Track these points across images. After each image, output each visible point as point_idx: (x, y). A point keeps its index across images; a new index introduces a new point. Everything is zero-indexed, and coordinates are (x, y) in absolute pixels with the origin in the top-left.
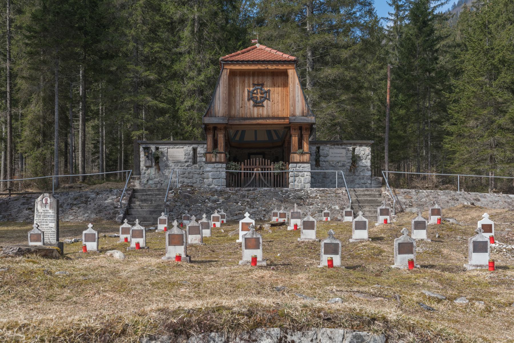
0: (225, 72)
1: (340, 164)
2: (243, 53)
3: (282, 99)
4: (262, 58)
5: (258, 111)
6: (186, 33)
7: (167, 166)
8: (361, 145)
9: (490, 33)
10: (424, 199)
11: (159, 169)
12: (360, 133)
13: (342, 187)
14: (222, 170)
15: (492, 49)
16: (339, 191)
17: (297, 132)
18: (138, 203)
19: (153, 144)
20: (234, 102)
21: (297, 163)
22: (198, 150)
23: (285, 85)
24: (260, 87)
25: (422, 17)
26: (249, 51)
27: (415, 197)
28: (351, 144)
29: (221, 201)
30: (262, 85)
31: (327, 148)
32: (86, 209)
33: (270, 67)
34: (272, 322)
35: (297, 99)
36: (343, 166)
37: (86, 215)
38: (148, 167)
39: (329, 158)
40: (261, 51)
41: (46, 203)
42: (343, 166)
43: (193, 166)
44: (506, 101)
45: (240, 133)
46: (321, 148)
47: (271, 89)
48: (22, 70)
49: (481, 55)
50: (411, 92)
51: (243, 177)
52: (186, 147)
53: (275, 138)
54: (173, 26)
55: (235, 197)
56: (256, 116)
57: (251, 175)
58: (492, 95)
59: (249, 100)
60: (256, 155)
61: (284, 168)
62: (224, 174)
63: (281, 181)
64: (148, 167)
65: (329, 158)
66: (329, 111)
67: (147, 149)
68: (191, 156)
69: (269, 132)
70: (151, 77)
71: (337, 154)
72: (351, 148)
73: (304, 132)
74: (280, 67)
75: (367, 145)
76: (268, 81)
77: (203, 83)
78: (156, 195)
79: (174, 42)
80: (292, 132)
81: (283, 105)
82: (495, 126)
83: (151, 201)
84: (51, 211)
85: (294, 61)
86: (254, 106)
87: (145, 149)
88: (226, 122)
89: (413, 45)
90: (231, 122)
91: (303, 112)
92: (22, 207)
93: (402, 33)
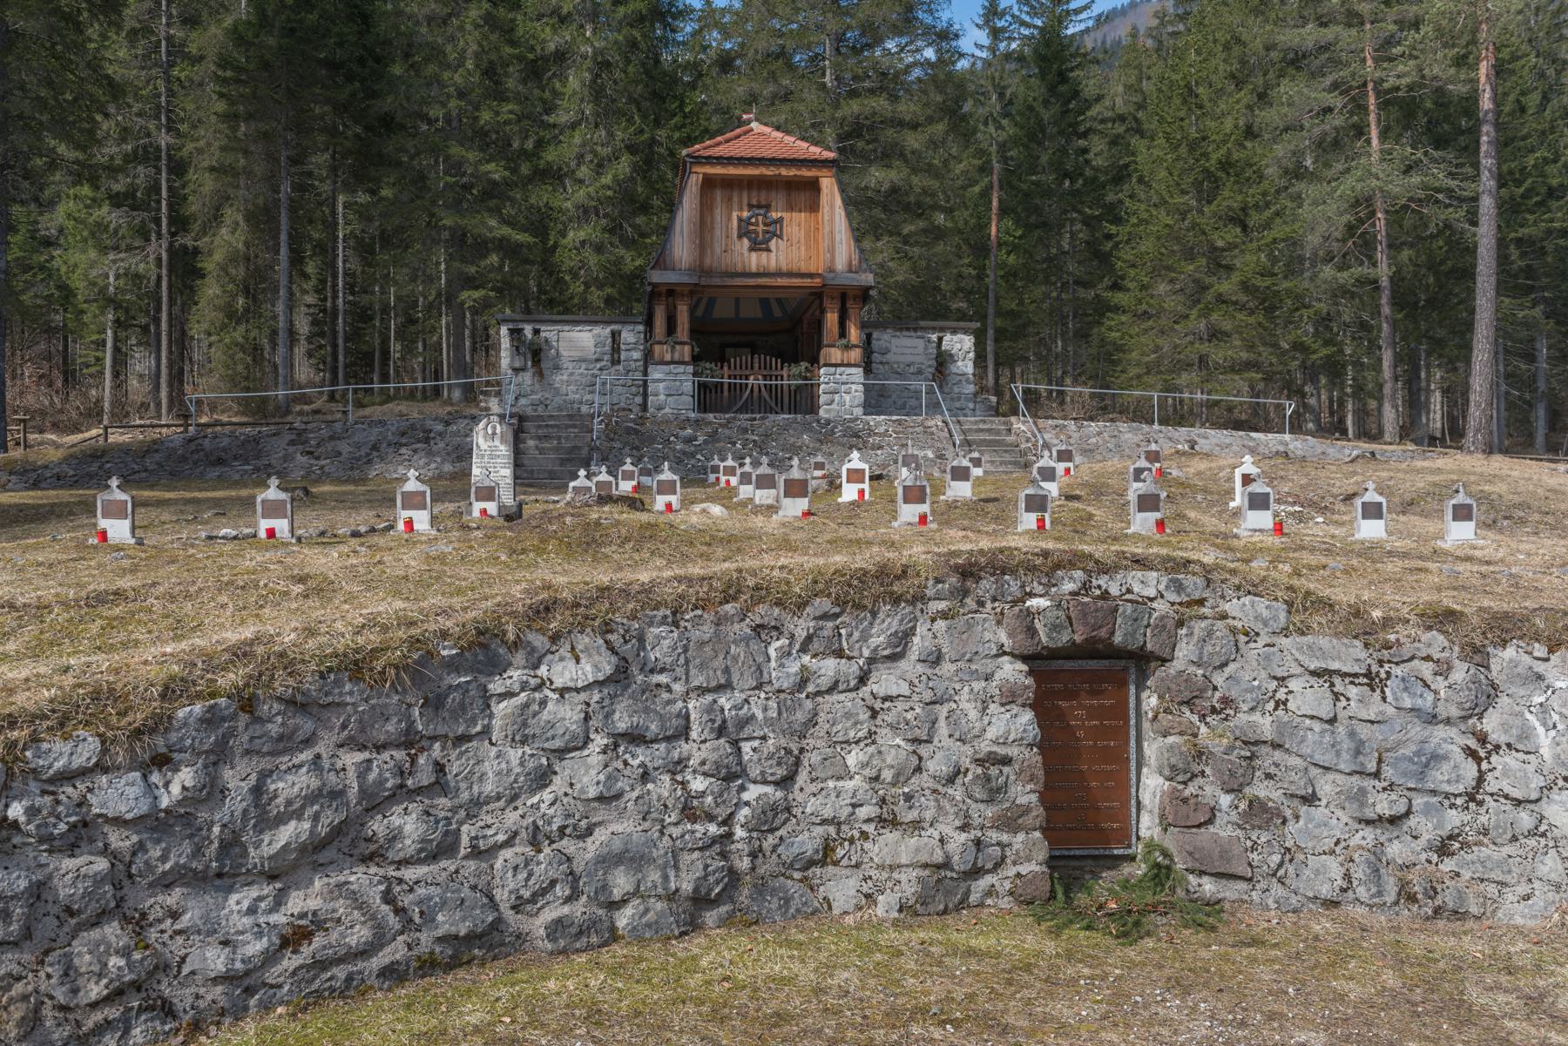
0: (694, 178)
1: (912, 370)
2: (727, 141)
4: (768, 154)
5: (758, 258)
6: (575, 81)
7: (557, 368)
8: (954, 331)
9: (1201, 107)
10: (1093, 440)
11: (540, 374)
13: (935, 413)
15: (1204, 139)
16: (931, 423)
17: (837, 305)
18: (531, 443)
19: (528, 322)
20: (701, 238)
21: (836, 365)
22: (623, 335)
23: (814, 207)
24: (762, 211)
25: (1054, 59)
26: (738, 137)
27: (1076, 435)
28: (934, 329)
30: (768, 207)
31: (886, 337)
32: (430, 454)
33: (784, 172)
34: (1072, 565)
35: (838, 239)
36: (920, 372)
37: (433, 466)
38: (516, 370)
39: (890, 357)
40: (762, 137)
41: (494, 433)
42: (920, 372)
43: (612, 370)
44: (1231, 246)
45: (704, 302)
46: (875, 335)
47: (784, 215)
48: (200, 151)
49: (1183, 150)
50: (1033, 219)
51: (726, 393)
52: (597, 330)
53: (777, 313)
54: (541, 68)
55: (727, 432)
56: (754, 269)
57: (743, 387)
58: (1204, 233)
59: (740, 237)
60: (756, 347)
61: (810, 375)
62: (688, 386)
63: (804, 401)
64: (516, 370)
65: (890, 357)
66: (879, 258)
67: (516, 333)
68: (608, 348)
69: (765, 302)
70: (497, 177)
71: (906, 348)
72: (934, 337)
74: (806, 173)
75: (966, 332)
76: (778, 199)
78: (568, 427)
79: (544, 102)
80: (827, 303)
81: (808, 248)
82: (1209, 296)
83: (559, 438)
84: (502, 447)
85: (833, 162)
86: (751, 249)
87: (512, 331)
88: (694, 280)
89: (1040, 121)
90: (704, 281)
91: (850, 264)
92: (291, 449)
93: (1005, 88)
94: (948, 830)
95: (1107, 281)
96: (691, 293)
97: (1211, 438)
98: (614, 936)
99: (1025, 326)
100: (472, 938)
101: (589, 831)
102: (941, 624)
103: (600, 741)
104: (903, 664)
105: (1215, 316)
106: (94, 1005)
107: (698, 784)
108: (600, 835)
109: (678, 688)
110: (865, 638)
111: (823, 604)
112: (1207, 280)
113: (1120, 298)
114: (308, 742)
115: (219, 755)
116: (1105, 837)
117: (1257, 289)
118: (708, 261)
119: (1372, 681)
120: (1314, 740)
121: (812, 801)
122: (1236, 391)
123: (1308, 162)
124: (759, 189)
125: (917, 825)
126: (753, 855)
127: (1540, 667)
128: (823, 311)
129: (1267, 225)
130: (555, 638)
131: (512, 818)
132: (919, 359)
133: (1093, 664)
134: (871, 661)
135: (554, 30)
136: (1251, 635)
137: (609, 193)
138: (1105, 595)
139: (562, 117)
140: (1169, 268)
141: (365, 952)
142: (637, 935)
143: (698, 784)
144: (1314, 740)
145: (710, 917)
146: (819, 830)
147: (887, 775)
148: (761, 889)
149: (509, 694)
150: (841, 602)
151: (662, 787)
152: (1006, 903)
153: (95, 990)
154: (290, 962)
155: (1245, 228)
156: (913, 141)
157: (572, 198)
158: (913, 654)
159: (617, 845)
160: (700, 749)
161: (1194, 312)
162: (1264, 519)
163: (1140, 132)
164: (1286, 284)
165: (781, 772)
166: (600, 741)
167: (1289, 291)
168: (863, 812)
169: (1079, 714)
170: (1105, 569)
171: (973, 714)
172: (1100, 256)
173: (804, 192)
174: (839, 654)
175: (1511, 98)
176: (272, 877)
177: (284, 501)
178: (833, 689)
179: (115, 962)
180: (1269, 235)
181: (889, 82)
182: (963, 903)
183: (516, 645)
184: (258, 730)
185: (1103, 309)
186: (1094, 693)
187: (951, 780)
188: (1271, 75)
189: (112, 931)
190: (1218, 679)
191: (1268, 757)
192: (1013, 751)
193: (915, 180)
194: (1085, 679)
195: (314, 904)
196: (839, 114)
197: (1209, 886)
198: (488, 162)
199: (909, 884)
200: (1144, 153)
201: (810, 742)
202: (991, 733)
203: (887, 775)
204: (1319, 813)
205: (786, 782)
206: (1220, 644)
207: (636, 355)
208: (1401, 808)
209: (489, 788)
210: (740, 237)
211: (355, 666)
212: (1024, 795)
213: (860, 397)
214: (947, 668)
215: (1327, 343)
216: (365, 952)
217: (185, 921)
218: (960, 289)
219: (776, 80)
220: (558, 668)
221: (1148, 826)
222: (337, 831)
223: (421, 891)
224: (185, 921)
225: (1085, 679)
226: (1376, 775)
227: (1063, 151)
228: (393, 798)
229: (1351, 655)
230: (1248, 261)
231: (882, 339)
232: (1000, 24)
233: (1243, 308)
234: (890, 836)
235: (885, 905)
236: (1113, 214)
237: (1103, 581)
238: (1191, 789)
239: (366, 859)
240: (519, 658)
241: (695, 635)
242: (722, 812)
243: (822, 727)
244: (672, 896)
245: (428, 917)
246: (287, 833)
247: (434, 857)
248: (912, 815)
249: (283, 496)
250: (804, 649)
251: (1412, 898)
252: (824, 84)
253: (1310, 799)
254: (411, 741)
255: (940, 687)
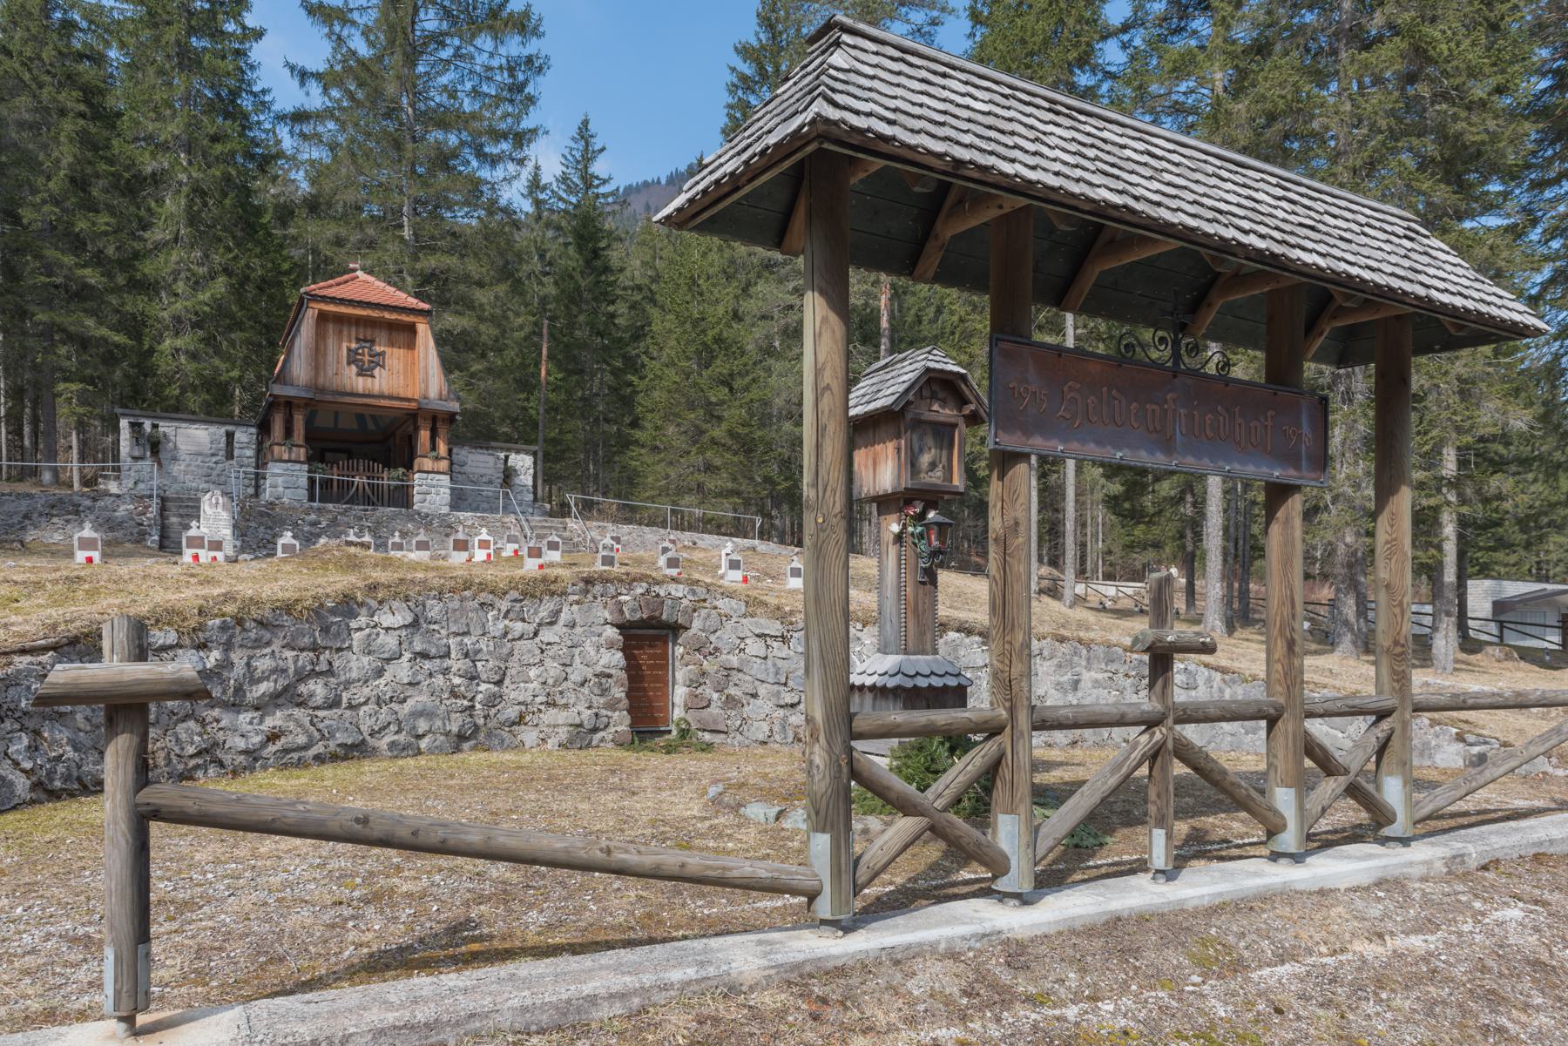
0: (310, 312)
3: (406, 366)
6: (173, 205)
7: (175, 459)
8: (518, 452)
12: (522, 437)
14: (301, 474)
16: (506, 520)
17: (429, 424)
18: (174, 520)
19: (147, 417)
22: (237, 435)
23: (411, 345)
28: (502, 449)
29: (324, 524)
30: (373, 342)
33: (387, 315)
34: (641, 580)
38: (135, 459)
39: (467, 469)
40: (366, 285)
44: (722, 402)
49: (688, 326)
52: (213, 429)
53: (371, 426)
56: (361, 391)
59: (349, 363)
60: (362, 452)
62: (304, 482)
63: (402, 497)
65: (467, 469)
67: (136, 427)
72: (502, 455)
73: (439, 425)
76: (382, 336)
77: (206, 309)
79: (140, 219)
80: (420, 422)
81: (406, 377)
82: (706, 438)
86: (359, 375)
87: (132, 425)
89: (578, 288)
94: (582, 709)
95: (627, 420)
96: (306, 405)
97: (708, 540)
98: (419, 753)
99: (563, 451)
100: (354, 746)
101: (404, 700)
102: (575, 607)
103: (407, 655)
104: (556, 627)
105: (709, 454)
106: (191, 757)
107: (457, 681)
108: (410, 702)
109: (443, 632)
110: (536, 613)
111: (515, 594)
112: (705, 427)
113: (638, 434)
114: (268, 644)
115: (228, 647)
116: (655, 721)
117: (739, 435)
118: (321, 381)
119: (784, 639)
120: (757, 668)
121: (511, 692)
122: (725, 512)
123: (777, 344)
124: (365, 326)
125: (566, 706)
126: (485, 717)
127: (859, 634)
128: (417, 429)
129: (747, 389)
130: (381, 603)
131: (366, 691)
132: (489, 472)
133: (651, 632)
134: (540, 625)
135: (153, 155)
136: (728, 617)
137: (206, 309)
138: (658, 595)
139: (157, 234)
140: (677, 415)
141: (305, 748)
142: (431, 751)
143: (457, 681)
144: (757, 668)
145: (466, 746)
146: (517, 708)
147: (550, 681)
148: (489, 735)
149: (360, 629)
150: (525, 594)
151: (439, 680)
152: (610, 745)
153: (191, 750)
154: (272, 748)
155: (731, 389)
156: (482, 296)
157: (164, 309)
158: (562, 621)
159: (420, 707)
160: (457, 663)
161: (694, 450)
162: (737, 575)
163: (653, 301)
164: (759, 433)
165: (497, 678)
166: (407, 655)
167: (762, 439)
168: (538, 700)
169: (644, 657)
170: (658, 583)
171: (593, 653)
172: (625, 400)
173: (404, 333)
174: (523, 620)
175: (913, 312)
176: (257, 709)
177: (95, 539)
178: (520, 638)
179: (196, 738)
180: (748, 396)
181: (458, 242)
182: (589, 746)
183: (361, 605)
184: (245, 635)
185: (626, 443)
186: (651, 646)
187: (582, 685)
188: (752, 275)
189: (191, 724)
190: (713, 638)
191: (736, 676)
192: (613, 671)
193: (483, 328)
194: (648, 637)
195: (278, 723)
196: (418, 266)
197: (707, 737)
198: (83, 267)
199: (563, 734)
200: (661, 323)
201: (510, 664)
202: (602, 662)
203: (550, 681)
204: (759, 702)
205: (499, 683)
206: (713, 621)
207: (249, 453)
208: (796, 700)
209: (354, 675)
210: (349, 363)
211: (288, 608)
212: (619, 693)
213: (447, 498)
214: (578, 630)
215: (786, 479)
216: (305, 748)
217: (223, 724)
218: (508, 417)
219: (362, 230)
220: (383, 617)
221: (678, 713)
222: (286, 689)
223: (327, 722)
224: (223, 724)
225: (648, 637)
226: (785, 684)
227: (595, 313)
228: (309, 676)
229: (775, 628)
230: (734, 414)
231: (462, 453)
232: (542, 196)
233: (729, 449)
234: (552, 711)
235: (552, 743)
236: (632, 365)
237: (656, 588)
238: (700, 690)
239: (299, 705)
240: (364, 611)
241: (451, 605)
242: (470, 695)
243: (516, 657)
244: (447, 734)
245: (332, 735)
246: (264, 687)
247: (330, 707)
248: (563, 701)
249: (95, 535)
250: (505, 617)
251: (800, 740)
252: (402, 238)
253: (755, 696)
254: (315, 648)
255: (576, 639)
